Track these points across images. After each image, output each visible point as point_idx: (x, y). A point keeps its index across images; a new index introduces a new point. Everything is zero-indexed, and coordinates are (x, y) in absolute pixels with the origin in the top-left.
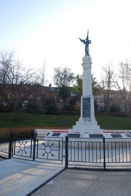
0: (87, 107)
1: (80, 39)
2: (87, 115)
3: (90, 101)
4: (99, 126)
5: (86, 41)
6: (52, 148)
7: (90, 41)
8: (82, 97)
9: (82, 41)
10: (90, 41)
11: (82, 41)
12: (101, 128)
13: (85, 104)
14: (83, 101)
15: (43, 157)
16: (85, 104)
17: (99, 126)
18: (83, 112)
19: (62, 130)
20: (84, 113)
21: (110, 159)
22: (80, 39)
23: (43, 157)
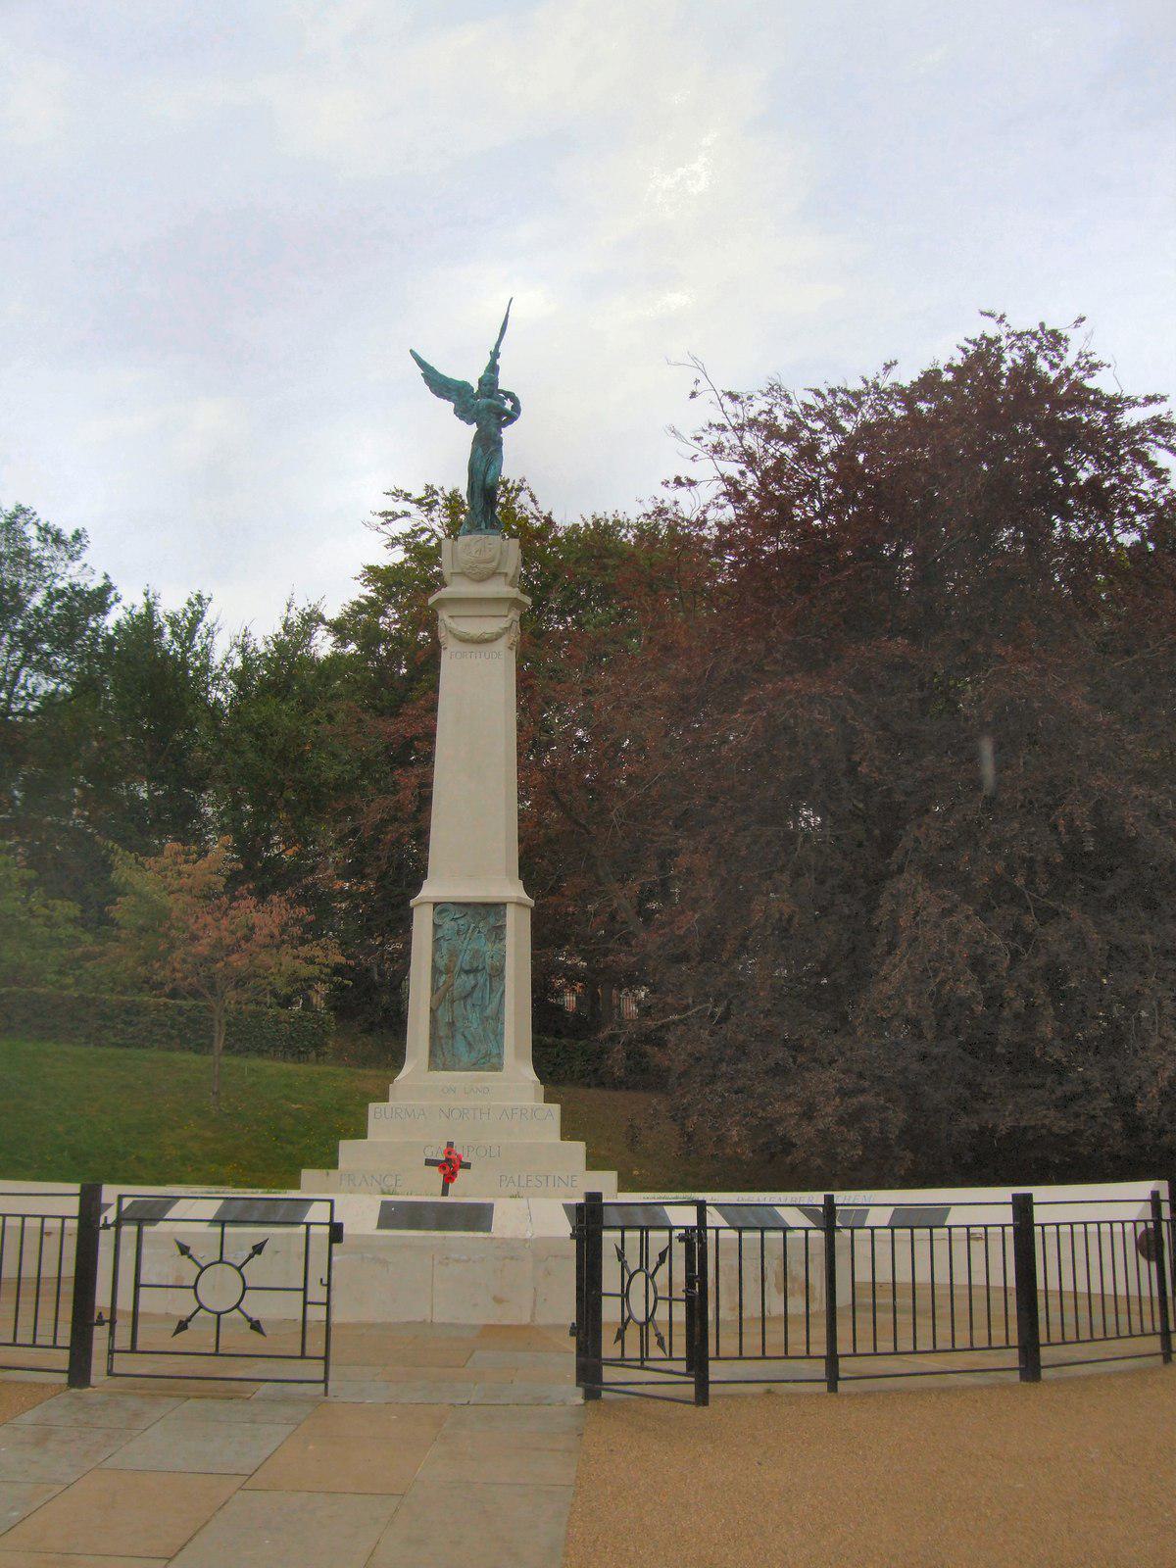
0: (468, 984)
1: (422, 364)
2: (463, 1044)
3: (498, 932)
4: (582, 1145)
5: (592, 527)
6: (256, 1272)
7: (508, 405)
8: (432, 890)
9: (440, 385)
10: (508, 405)
11: (440, 385)
12: (361, 1133)
13: (453, 954)
14: (436, 927)
15: (184, 1341)
16: (453, 954)
17: (582, 1145)
18: (434, 1021)
19: (671, 1196)
20: (443, 1032)
21: (944, 1331)
22: (422, 364)
23: (184, 1341)
